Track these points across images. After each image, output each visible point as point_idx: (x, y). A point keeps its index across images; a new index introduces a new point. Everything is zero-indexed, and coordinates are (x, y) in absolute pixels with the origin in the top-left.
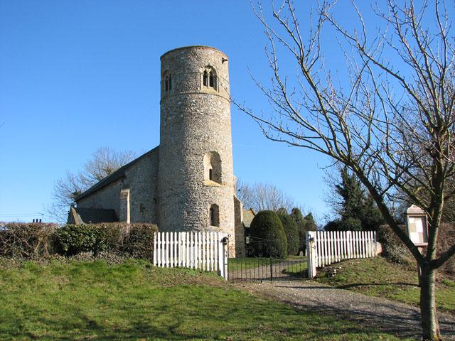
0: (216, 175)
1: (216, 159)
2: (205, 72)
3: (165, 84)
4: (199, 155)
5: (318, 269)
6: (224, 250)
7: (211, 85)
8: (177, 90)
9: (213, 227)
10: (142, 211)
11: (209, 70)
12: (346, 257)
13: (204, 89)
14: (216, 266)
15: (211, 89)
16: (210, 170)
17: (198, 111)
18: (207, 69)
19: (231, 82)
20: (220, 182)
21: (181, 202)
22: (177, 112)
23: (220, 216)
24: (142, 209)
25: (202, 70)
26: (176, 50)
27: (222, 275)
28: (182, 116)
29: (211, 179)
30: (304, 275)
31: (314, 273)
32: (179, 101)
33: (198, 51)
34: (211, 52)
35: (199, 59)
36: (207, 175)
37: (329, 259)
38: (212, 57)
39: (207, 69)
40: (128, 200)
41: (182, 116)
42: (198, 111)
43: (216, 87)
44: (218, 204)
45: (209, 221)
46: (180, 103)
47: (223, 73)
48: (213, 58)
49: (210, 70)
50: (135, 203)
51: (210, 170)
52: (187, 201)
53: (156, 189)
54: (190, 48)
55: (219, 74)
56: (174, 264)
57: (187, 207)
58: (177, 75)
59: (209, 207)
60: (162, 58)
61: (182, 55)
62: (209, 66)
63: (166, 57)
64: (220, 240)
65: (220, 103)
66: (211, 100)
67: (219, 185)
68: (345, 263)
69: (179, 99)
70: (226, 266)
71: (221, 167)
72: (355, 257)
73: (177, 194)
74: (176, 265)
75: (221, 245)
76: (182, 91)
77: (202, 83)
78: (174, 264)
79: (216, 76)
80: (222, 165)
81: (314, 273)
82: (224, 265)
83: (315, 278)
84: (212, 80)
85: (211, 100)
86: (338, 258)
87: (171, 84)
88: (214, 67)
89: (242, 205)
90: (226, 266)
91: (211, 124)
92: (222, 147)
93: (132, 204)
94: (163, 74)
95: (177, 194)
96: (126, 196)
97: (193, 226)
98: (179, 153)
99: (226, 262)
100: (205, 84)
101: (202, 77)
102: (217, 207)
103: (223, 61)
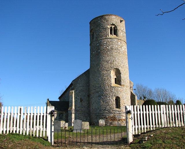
0: (118, 81)
1: (118, 73)
2: (111, 28)
3: (91, 36)
4: (109, 71)
5: (135, 136)
6: (51, 120)
7: (115, 34)
8: (97, 38)
9: (117, 109)
10: (81, 102)
11: (113, 27)
12: (160, 126)
13: (110, 36)
14: (44, 133)
15: (114, 36)
16: (115, 78)
17: (107, 47)
18: (112, 26)
19: (127, 32)
20: (120, 85)
21: (100, 96)
22: (98, 51)
23: (121, 103)
24: (81, 100)
25: (109, 27)
26: (96, 18)
27: (49, 140)
28: (99, 51)
29: (116, 83)
30: (124, 140)
31: (131, 139)
32: (98, 43)
33: (107, 17)
34: (113, 17)
35: (107, 21)
36: (113, 81)
37: (145, 127)
38: (115, 19)
39: (112, 26)
40: (73, 96)
41: (99, 51)
42: (107, 47)
43: (117, 35)
44: (119, 96)
45: (115, 106)
46: (98, 44)
47: (122, 27)
48: (115, 20)
49: (114, 26)
50: (78, 97)
51: (115, 78)
52: (103, 96)
53: (89, 90)
54: (103, 16)
55: (118, 28)
56: (9, 131)
57: (103, 99)
58: (97, 31)
59: (114, 98)
60: (90, 23)
61: (99, 20)
62: (113, 25)
63: (92, 22)
64: (48, 112)
65: (119, 43)
66: (114, 42)
67: (120, 86)
68: (158, 132)
69: (97, 42)
70: (53, 133)
71: (121, 77)
72: (169, 126)
73: (98, 92)
74: (11, 132)
75: (49, 117)
76: (99, 38)
77: (109, 33)
78: (9, 131)
79: (117, 29)
80: (122, 76)
81: (131, 139)
82: (51, 132)
83: (131, 143)
84: (115, 31)
85: (114, 42)
86: (152, 127)
87: (94, 35)
88: (116, 25)
89: (136, 97)
90: (53, 133)
91: (114, 54)
92: (121, 66)
93: (75, 98)
94: (91, 31)
95: (98, 92)
96: (72, 94)
97: (106, 109)
98: (98, 70)
99: (53, 130)
100: (111, 34)
101: (109, 30)
102: (119, 98)
103: (121, 21)
